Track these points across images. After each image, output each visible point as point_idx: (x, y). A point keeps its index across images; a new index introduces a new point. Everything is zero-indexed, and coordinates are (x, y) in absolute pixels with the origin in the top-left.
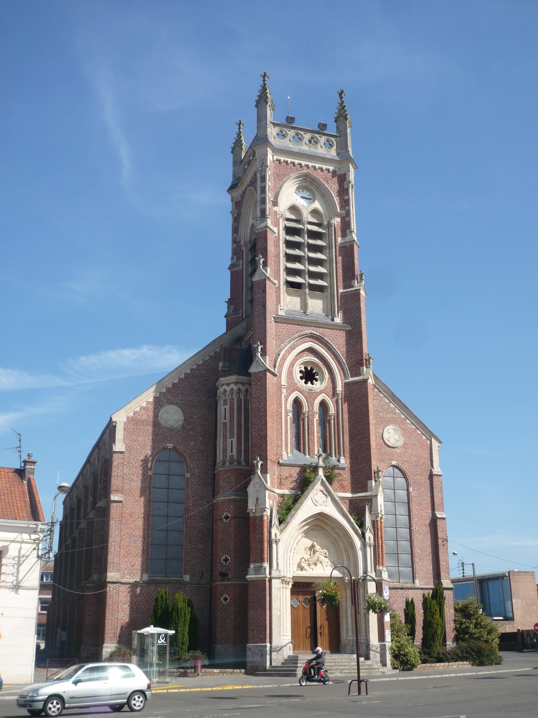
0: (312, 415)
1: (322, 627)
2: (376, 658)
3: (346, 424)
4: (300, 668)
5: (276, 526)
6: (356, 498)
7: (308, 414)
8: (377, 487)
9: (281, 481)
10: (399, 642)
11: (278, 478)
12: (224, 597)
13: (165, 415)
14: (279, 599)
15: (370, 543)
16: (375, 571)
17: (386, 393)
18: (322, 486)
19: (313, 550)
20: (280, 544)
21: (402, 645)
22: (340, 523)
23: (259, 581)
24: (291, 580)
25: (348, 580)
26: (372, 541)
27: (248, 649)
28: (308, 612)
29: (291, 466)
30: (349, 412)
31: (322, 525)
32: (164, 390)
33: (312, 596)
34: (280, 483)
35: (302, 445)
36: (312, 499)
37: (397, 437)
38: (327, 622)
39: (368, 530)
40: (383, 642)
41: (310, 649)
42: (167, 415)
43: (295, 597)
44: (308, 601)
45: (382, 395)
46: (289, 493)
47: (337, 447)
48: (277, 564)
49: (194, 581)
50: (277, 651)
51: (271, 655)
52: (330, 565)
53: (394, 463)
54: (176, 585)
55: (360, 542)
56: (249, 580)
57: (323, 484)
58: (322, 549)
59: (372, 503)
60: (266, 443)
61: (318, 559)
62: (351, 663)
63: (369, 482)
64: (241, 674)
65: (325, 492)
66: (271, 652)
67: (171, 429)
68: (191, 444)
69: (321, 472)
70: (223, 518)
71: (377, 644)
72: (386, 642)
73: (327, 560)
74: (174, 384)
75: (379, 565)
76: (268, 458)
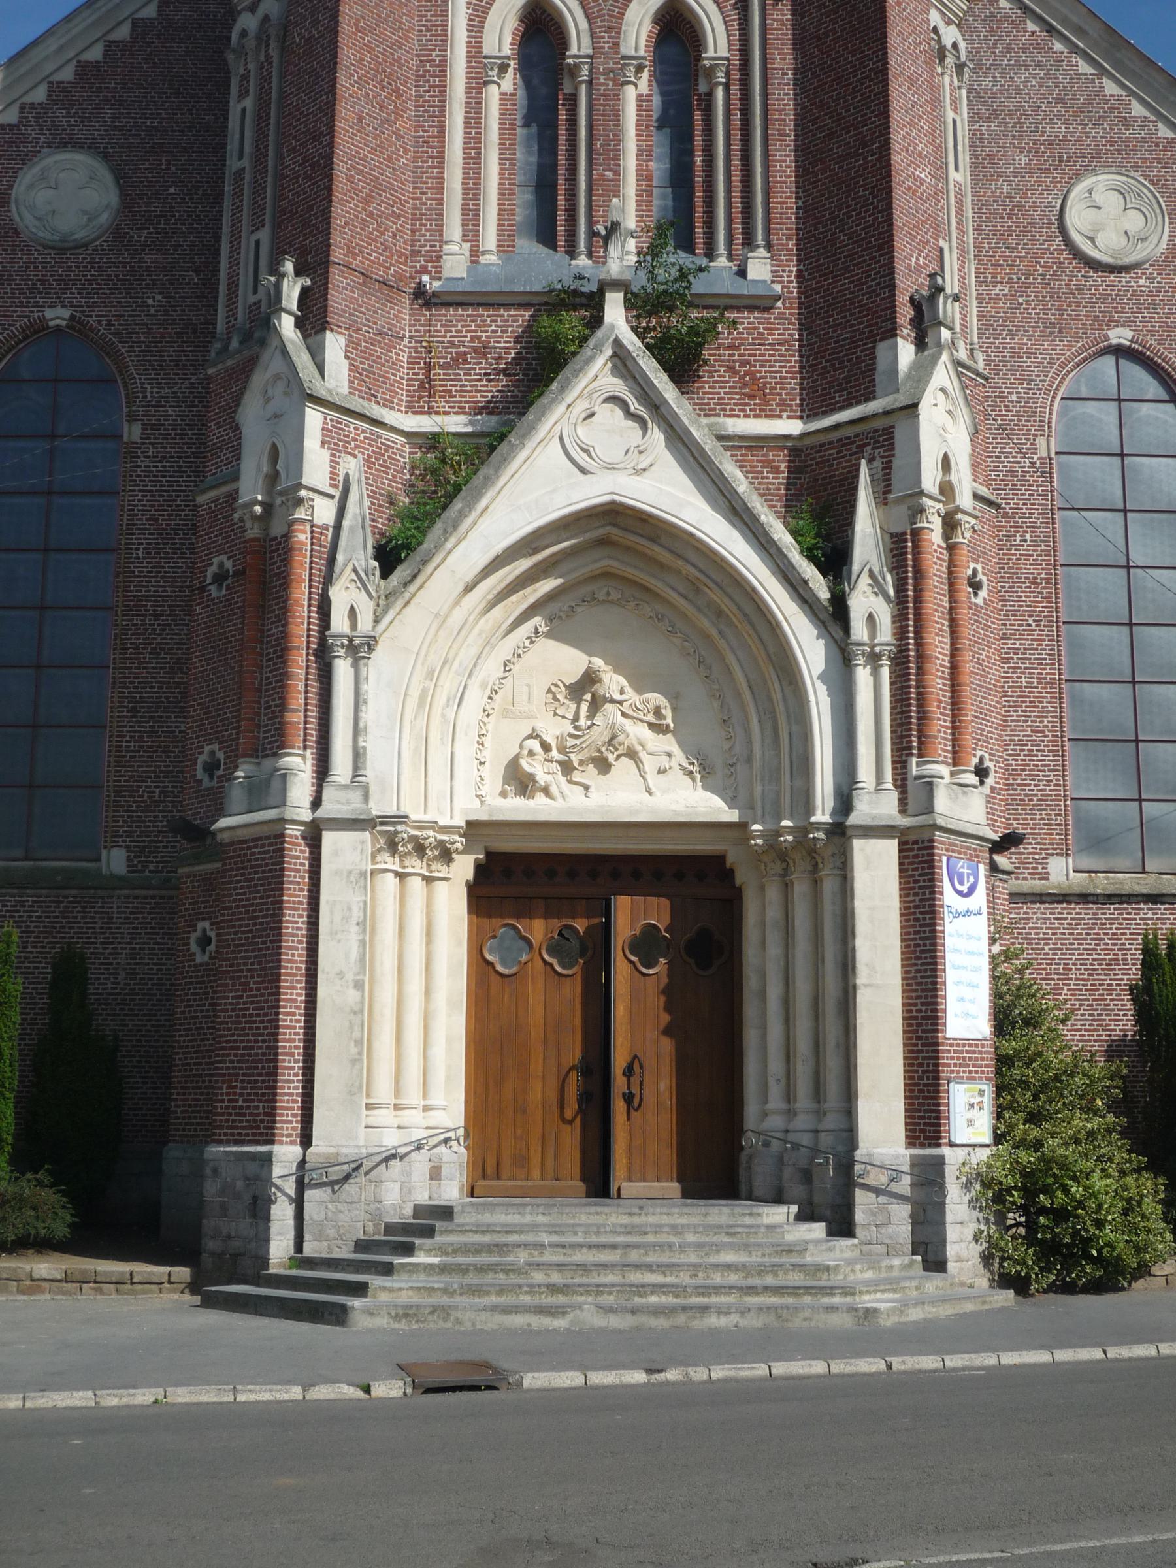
0: (612, 71)
1: (636, 1067)
2: (890, 1230)
3: (784, 98)
4: (405, 1277)
5: (355, 570)
6: (822, 438)
7: (591, 71)
8: (922, 372)
9: (428, 377)
10: (1037, 1145)
11: (412, 362)
12: (199, 933)
13: (41, 197)
14: (355, 929)
15: (873, 647)
16: (901, 783)
17: (1080, 32)
18: (622, 377)
19: (588, 697)
20: (380, 662)
21: (1047, 1161)
22: (723, 559)
23: (260, 839)
24: (457, 838)
25: (762, 834)
26: (886, 633)
27: (208, 1171)
28: (573, 991)
29: (486, 305)
30: (801, 43)
31: (630, 572)
32: (40, 95)
33: (595, 921)
34: (422, 386)
35: (561, 217)
36: (561, 438)
37: (1134, 222)
38: (667, 1046)
39: (864, 581)
40: (930, 1145)
41: (578, 1176)
42: (50, 192)
43: (507, 925)
44: (575, 943)
45: (1058, 46)
46: (469, 429)
47: (737, 207)
48: (358, 756)
49: (147, 873)
50: (332, 1184)
51: (299, 1203)
52: (683, 769)
53: (1120, 336)
54: (67, 892)
55: (821, 642)
56: (226, 837)
57: (625, 365)
58: (640, 690)
59: (891, 447)
60: (329, 190)
61: (613, 737)
62: (718, 1251)
63: (882, 348)
64: (174, 1291)
65: (634, 405)
66: (301, 1186)
67: (63, 249)
68: (150, 302)
69: (615, 312)
70: (209, 580)
71: (897, 1157)
72: (952, 1145)
73: (668, 743)
74: (84, 69)
75: (920, 756)
76: (338, 254)
